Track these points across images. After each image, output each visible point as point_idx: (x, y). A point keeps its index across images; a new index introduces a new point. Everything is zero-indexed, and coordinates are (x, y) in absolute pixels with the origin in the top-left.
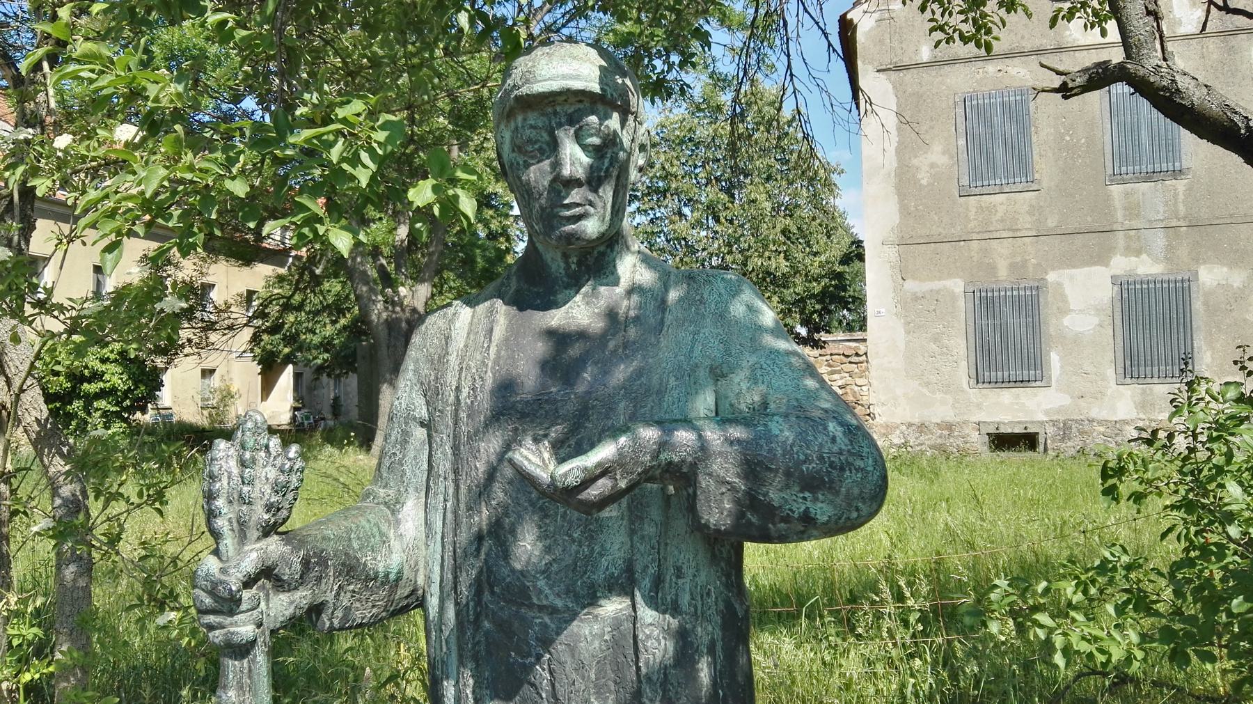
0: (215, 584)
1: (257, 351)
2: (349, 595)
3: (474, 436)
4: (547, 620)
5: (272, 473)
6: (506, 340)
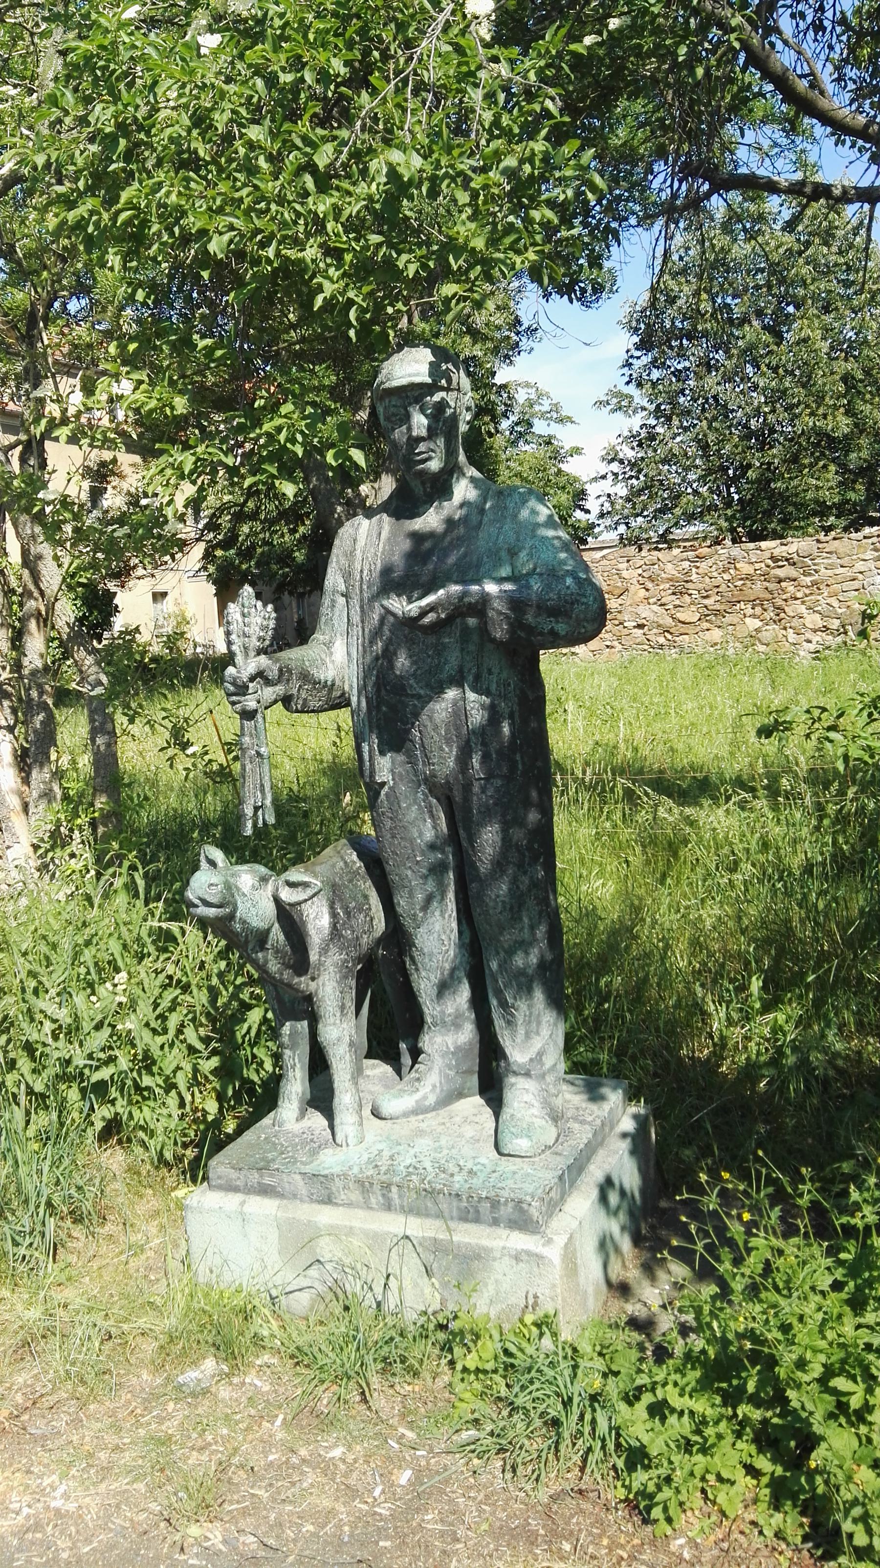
0: (235, 679)
1: (211, 569)
5: (259, 620)
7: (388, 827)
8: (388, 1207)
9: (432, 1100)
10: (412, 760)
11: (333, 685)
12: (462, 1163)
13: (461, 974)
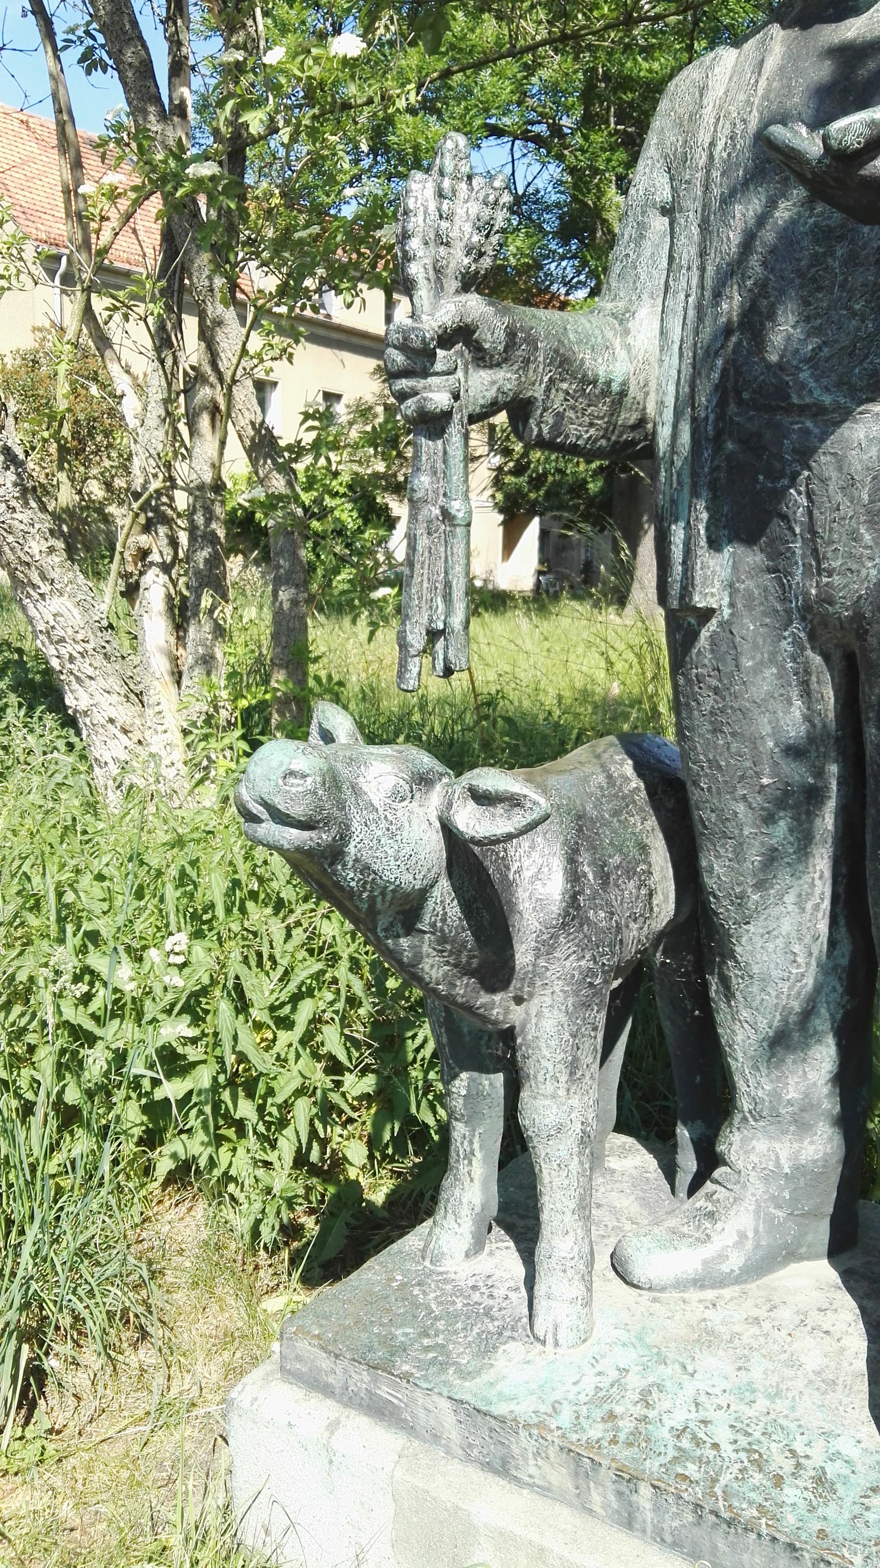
2: (561, 396)
3: (727, 200)
4: (809, 424)
5: (474, 208)
6: (781, 69)
7: (707, 708)
8: (628, 1520)
9: (735, 1262)
10: (778, 565)
11: (623, 394)
12: (799, 1447)
13: (822, 1022)
